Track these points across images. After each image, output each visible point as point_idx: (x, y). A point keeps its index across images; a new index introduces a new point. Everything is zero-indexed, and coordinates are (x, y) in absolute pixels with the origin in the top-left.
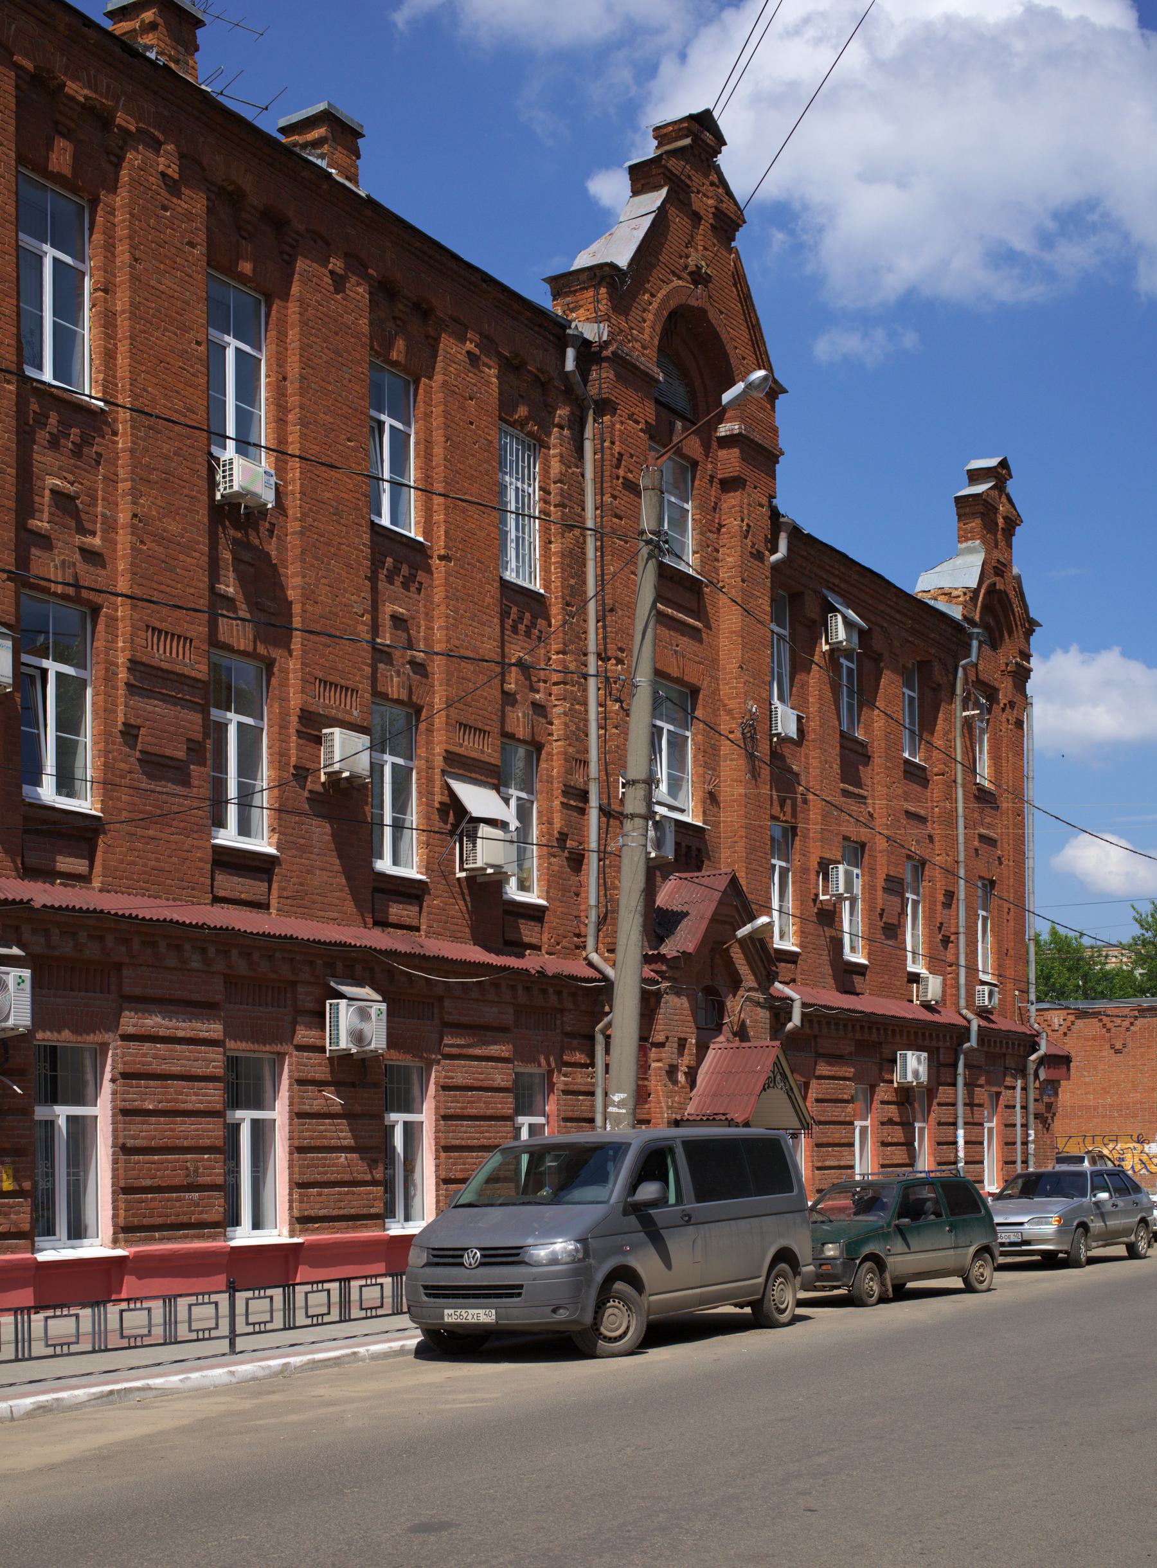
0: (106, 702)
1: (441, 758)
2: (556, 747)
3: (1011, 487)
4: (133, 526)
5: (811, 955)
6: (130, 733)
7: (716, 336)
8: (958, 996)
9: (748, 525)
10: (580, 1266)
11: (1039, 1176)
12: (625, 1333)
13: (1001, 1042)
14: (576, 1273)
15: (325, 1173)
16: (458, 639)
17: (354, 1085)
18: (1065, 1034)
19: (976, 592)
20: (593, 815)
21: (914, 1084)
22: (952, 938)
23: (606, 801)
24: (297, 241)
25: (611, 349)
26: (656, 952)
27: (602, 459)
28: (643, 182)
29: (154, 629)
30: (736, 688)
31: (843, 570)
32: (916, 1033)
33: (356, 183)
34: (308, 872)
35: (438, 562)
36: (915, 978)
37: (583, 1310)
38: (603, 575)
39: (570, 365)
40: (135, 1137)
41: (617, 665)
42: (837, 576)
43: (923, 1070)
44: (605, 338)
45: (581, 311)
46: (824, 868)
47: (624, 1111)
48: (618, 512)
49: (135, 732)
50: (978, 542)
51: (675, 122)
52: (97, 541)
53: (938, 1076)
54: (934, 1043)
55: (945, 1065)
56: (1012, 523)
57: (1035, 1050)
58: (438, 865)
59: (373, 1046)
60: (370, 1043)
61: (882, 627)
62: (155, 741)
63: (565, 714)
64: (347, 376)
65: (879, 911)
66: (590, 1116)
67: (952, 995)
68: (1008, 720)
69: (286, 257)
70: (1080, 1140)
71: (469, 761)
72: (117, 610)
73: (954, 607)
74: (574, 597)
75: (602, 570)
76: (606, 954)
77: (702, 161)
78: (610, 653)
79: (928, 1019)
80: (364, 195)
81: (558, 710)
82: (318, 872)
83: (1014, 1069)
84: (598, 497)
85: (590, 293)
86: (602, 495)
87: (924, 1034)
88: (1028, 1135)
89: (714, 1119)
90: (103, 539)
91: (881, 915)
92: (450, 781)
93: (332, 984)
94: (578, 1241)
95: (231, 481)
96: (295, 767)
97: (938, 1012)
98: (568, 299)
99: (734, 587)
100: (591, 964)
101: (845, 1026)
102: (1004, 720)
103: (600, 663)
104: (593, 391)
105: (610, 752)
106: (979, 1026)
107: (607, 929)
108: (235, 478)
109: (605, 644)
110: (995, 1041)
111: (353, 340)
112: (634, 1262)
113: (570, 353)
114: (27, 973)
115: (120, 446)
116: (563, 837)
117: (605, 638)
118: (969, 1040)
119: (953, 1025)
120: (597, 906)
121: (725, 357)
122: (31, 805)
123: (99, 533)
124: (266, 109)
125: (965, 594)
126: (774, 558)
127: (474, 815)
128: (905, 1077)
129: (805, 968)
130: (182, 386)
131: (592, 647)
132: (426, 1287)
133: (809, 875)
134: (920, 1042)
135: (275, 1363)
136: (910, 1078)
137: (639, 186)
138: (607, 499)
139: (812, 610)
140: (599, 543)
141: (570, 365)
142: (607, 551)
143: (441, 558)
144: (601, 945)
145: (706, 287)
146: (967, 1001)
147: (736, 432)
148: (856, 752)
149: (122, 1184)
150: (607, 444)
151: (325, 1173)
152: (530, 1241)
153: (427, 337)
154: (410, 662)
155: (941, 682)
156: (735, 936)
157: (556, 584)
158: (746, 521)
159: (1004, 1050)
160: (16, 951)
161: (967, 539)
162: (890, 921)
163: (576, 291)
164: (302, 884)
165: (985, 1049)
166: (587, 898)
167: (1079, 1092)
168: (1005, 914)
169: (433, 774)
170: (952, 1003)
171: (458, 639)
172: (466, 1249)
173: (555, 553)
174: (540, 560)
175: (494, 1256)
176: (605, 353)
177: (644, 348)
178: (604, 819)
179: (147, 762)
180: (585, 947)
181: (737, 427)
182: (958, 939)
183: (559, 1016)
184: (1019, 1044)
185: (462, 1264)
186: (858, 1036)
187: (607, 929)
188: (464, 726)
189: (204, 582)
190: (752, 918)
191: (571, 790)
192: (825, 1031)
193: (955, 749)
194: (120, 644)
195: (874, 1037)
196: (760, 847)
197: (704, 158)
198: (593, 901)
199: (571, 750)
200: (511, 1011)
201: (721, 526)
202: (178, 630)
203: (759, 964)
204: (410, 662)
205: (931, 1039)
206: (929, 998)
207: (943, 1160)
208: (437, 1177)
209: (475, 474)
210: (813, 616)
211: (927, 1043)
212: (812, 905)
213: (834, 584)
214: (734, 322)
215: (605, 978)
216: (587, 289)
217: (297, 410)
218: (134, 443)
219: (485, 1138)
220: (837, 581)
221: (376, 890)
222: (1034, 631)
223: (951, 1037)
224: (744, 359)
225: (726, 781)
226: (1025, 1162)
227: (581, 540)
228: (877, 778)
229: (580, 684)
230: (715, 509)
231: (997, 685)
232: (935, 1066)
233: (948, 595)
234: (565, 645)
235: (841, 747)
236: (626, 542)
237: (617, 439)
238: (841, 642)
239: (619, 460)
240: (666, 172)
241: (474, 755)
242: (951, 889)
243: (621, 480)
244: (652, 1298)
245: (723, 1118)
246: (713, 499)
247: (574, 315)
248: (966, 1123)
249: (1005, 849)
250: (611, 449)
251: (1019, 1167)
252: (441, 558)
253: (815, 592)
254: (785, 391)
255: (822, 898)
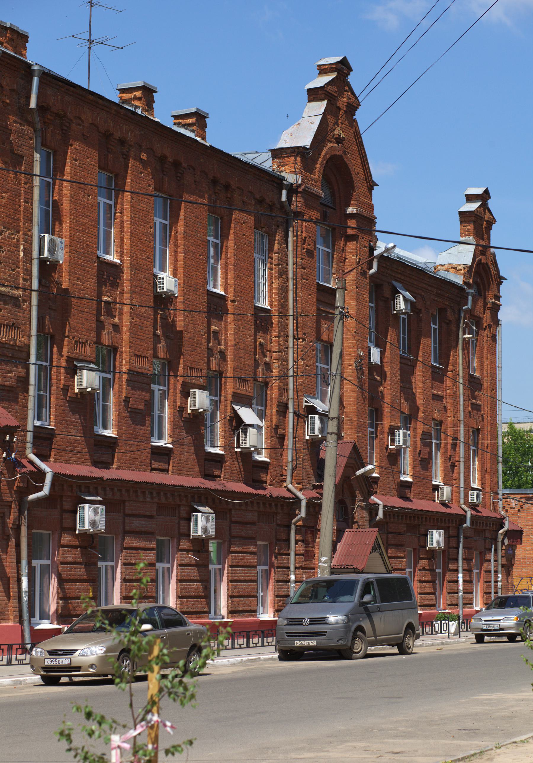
0: (119, 388)
1: (231, 395)
2: (275, 384)
3: (491, 203)
4: (131, 313)
5: (384, 478)
6: (127, 400)
7: (347, 166)
8: (459, 497)
9: (359, 259)
10: (347, 625)
11: (507, 598)
12: (361, 651)
13: (483, 523)
14: (346, 627)
15: (189, 592)
16: (238, 339)
17: (199, 551)
18: (519, 511)
19: (471, 267)
20: (291, 416)
21: (437, 548)
22: (457, 463)
23: (296, 409)
24: (183, 171)
25: (303, 187)
26: (319, 484)
27: (297, 240)
28: (314, 96)
29: (136, 355)
30: (352, 343)
31: (402, 270)
32: (437, 519)
33: (206, 141)
34: (183, 454)
35: (230, 303)
36: (436, 488)
37: (348, 641)
38: (296, 297)
39: (284, 198)
40: (128, 575)
41: (303, 342)
42: (400, 273)
43: (442, 540)
44: (300, 182)
45: (287, 167)
46: (392, 431)
47: (326, 565)
48: (304, 266)
49: (128, 400)
50: (472, 237)
51: (329, 64)
52: (116, 320)
53: (449, 543)
54: (447, 525)
55: (452, 537)
56: (491, 222)
57: (502, 527)
58: (228, 447)
59: (210, 534)
60: (209, 533)
61: (421, 295)
62: (135, 403)
63: (279, 367)
64: (200, 227)
65: (418, 451)
66: (287, 565)
67: (456, 496)
68: (488, 335)
69: (178, 178)
70: (529, 580)
71: (242, 396)
72: (122, 348)
73: (459, 276)
74: (283, 307)
75: (296, 295)
76: (296, 485)
77: (341, 80)
78: (299, 336)
79: (444, 511)
80: (208, 145)
81: (275, 365)
82: (185, 454)
83: (490, 539)
84: (295, 259)
85: (292, 159)
86: (297, 258)
87: (441, 520)
88: (498, 577)
89: (347, 568)
90: (119, 319)
91: (419, 454)
92: (236, 407)
93: (195, 506)
94: (346, 616)
95: (163, 287)
96: (179, 407)
97: (450, 507)
98: (281, 160)
99: (352, 291)
100: (289, 490)
101: (402, 516)
102: (485, 335)
103: (295, 341)
104: (293, 207)
105: (299, 385)
106: (471, 514)
107: (297, 473)
108: (165, 285)
109: (297, 331)
110: (480, 523)
111: (202, 210)
112: (363, 624)
113: (284, 192)
114: (103, 507)
115: (125, 278)
116: (277, 427)
117: (297, 328)
118: (465, 523)
119: (457, 514)
120: (292, 461)
121: (350, 175)
122: (97, 435)
123: (117, 316)
124: (122, 48)
125: (464, 268)
126: (372, 271)
127: (247, 423)
128: (432, 544)
129: (382, 485)
130: (146, 248)
131: (291, 333)
132: (287, 633)
133: (384, 435)
134: (439, 524)
135: (239, 659)
136: (435, 545)
137: (312, 98)
138: (299, 260)
139: (387, 293)
140: (295, 282)
141: (284, 198)
142: (299, 286)
143: (231, 301)
144: (293, 481)
145: (342, 144)
146: (465, 500)
147: (355, 212)
148: (407, 365)
149: (124, 595)
150: (299, 233)
151: (189, 592)
152: (328, 616)
153: (227, 198)
154: (219, 352)
155: (451, 319)
156: (355, 474)
157: (275, 303)
158: (358, 256)
159: (484, 528)
160: (99, 498)
161: (465, 235)
162: (424, 457)
163: (285, 157)
164: (180, 460)
165: (474, 527)
166: (287, 456)
167: (528, 549)
168: (485, 447)
169: (227, 403)
170: (456, 501)
171: (238, 339)
172: (303, 619)
173: (275, 288)
174: (268, 292)
175: (314, 621)
176: (300, 190)
177: (316, 182)
178: (296, 418)
179: (133, 412)
180: (285, 481)
181: (355, 210)
182: (459, 464)
183: (275, 516)
184: (493, 524)
185: (302, 624)
186: (408, 522)
187: (297, 473)
188: (240, 379)
189: (151, 331)
190: (363, 466)
191: (281, 404)
192: (392, 520)
193: (459, 356)
194: (124, 363)
195: (416, 522)
196: (363, 424)
197: (342, 79)
198: (290, 459)
199: (281, 384)
200: (256, 514)
201: (345, 259)
202: (144, 354)
203: (365, 487)
204: (219, 352)
205: (445, 523)
206: (444, 499)
207: (451, 591)
208: (228, 595)
209: (245, 258)
210: (388, 296)
211: (443, 525)
212: (385, 451)
213: (398, 278)
214: (354, 156)
215: (297, 497)
216: (290, 157)
217: (182, 247)
218: (131, 277)
219: (246, 576)
220: (399, 276)
221: (206, 460)
222: (502, 282)
223: (456, 521)
224: (358, 173)
225: (347, 391)
226: (496, 593)
227: (286, 280)
228: (418, 378)
229: (285, 351)
230: (343, 250)
231: (481, 316)
232: (447, 538)
233: (455, 269)
234: (279, 333)
235: (401, 363)
236: (307, 280)
237: (304, 230)
238: (402, 310)
239: (305, 240)
240: (327, 93)
241: (244, 393)
242: (456, 436)
243: (305, 250)
244: (368, 639)
245: (352, 567)
246: (342, 245)
247: (283, 168)
248: (464, 570)
249: (486, 410)
250: (301, 235)
251: (493, 595)
252: (231, 301)
253: (389, 283)
254: (377, 185)
255: (390, 447)
